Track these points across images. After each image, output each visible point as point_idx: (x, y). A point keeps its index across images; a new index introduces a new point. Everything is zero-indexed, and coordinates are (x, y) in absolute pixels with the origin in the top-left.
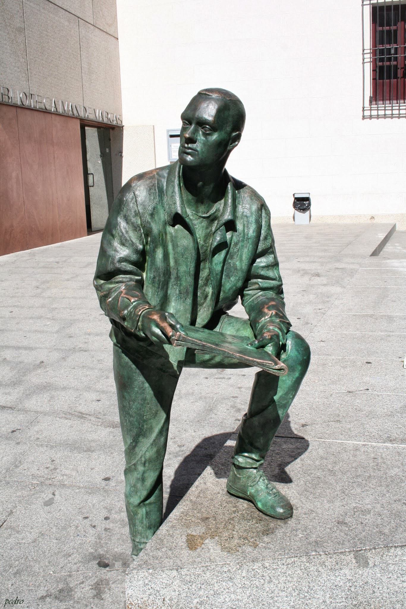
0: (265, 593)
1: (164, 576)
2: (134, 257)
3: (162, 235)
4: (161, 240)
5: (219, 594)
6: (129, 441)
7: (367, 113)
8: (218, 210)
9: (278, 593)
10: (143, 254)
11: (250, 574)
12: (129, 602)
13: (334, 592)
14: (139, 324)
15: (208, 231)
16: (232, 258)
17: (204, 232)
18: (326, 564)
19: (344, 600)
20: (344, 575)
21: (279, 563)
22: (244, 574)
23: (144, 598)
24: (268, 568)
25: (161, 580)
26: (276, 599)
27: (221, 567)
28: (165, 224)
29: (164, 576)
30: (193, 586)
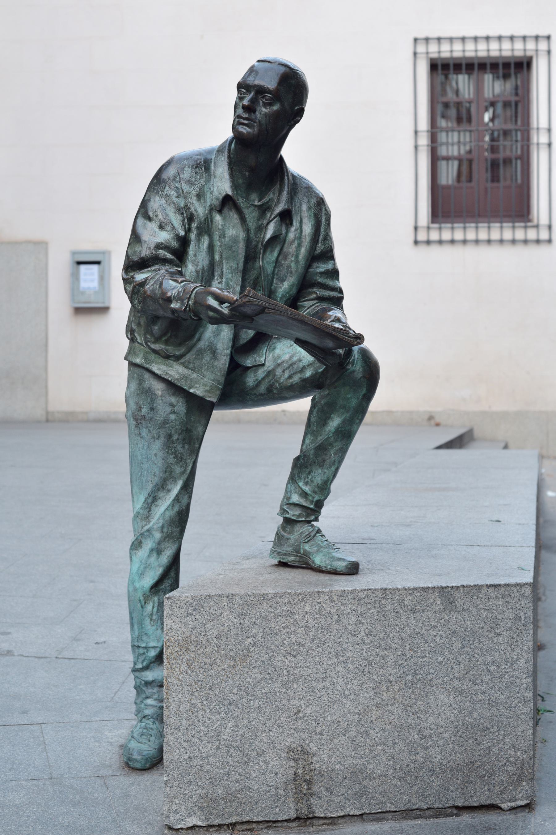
0: (332, 637)
1: (211, 603)
2: (174, 244)
3: (208, 221)
4: (206, 228)
5: (276, 634)
6: (141, 499)
7: (422, 236)
8: (271, 200)
9: (348, 638)
10: (184, 242)
11: (314, 608)
12: (167, 637)
13: (415, 642)
14: (190, 302)
15: (260, 223)
16: (286, 258)
17: (255, 224)
18: (406, 603)
19: (427, 655)
20: (427, 620)
21: (349, 597)
22: (307, 609)
23: (186, 633)
24: (337, 602)
25: (208, 609)
26: (345, 646)
27: (280, 597)
28: (211, 209)
29: (211, 603)
30: (246, 621)
